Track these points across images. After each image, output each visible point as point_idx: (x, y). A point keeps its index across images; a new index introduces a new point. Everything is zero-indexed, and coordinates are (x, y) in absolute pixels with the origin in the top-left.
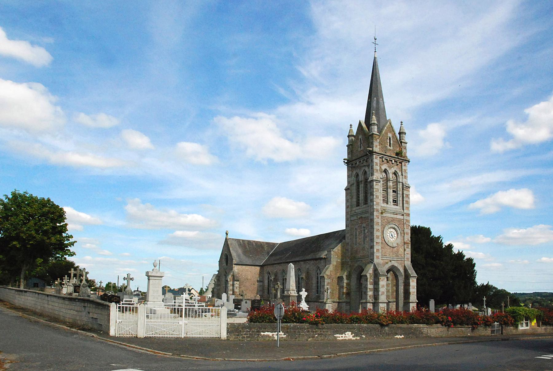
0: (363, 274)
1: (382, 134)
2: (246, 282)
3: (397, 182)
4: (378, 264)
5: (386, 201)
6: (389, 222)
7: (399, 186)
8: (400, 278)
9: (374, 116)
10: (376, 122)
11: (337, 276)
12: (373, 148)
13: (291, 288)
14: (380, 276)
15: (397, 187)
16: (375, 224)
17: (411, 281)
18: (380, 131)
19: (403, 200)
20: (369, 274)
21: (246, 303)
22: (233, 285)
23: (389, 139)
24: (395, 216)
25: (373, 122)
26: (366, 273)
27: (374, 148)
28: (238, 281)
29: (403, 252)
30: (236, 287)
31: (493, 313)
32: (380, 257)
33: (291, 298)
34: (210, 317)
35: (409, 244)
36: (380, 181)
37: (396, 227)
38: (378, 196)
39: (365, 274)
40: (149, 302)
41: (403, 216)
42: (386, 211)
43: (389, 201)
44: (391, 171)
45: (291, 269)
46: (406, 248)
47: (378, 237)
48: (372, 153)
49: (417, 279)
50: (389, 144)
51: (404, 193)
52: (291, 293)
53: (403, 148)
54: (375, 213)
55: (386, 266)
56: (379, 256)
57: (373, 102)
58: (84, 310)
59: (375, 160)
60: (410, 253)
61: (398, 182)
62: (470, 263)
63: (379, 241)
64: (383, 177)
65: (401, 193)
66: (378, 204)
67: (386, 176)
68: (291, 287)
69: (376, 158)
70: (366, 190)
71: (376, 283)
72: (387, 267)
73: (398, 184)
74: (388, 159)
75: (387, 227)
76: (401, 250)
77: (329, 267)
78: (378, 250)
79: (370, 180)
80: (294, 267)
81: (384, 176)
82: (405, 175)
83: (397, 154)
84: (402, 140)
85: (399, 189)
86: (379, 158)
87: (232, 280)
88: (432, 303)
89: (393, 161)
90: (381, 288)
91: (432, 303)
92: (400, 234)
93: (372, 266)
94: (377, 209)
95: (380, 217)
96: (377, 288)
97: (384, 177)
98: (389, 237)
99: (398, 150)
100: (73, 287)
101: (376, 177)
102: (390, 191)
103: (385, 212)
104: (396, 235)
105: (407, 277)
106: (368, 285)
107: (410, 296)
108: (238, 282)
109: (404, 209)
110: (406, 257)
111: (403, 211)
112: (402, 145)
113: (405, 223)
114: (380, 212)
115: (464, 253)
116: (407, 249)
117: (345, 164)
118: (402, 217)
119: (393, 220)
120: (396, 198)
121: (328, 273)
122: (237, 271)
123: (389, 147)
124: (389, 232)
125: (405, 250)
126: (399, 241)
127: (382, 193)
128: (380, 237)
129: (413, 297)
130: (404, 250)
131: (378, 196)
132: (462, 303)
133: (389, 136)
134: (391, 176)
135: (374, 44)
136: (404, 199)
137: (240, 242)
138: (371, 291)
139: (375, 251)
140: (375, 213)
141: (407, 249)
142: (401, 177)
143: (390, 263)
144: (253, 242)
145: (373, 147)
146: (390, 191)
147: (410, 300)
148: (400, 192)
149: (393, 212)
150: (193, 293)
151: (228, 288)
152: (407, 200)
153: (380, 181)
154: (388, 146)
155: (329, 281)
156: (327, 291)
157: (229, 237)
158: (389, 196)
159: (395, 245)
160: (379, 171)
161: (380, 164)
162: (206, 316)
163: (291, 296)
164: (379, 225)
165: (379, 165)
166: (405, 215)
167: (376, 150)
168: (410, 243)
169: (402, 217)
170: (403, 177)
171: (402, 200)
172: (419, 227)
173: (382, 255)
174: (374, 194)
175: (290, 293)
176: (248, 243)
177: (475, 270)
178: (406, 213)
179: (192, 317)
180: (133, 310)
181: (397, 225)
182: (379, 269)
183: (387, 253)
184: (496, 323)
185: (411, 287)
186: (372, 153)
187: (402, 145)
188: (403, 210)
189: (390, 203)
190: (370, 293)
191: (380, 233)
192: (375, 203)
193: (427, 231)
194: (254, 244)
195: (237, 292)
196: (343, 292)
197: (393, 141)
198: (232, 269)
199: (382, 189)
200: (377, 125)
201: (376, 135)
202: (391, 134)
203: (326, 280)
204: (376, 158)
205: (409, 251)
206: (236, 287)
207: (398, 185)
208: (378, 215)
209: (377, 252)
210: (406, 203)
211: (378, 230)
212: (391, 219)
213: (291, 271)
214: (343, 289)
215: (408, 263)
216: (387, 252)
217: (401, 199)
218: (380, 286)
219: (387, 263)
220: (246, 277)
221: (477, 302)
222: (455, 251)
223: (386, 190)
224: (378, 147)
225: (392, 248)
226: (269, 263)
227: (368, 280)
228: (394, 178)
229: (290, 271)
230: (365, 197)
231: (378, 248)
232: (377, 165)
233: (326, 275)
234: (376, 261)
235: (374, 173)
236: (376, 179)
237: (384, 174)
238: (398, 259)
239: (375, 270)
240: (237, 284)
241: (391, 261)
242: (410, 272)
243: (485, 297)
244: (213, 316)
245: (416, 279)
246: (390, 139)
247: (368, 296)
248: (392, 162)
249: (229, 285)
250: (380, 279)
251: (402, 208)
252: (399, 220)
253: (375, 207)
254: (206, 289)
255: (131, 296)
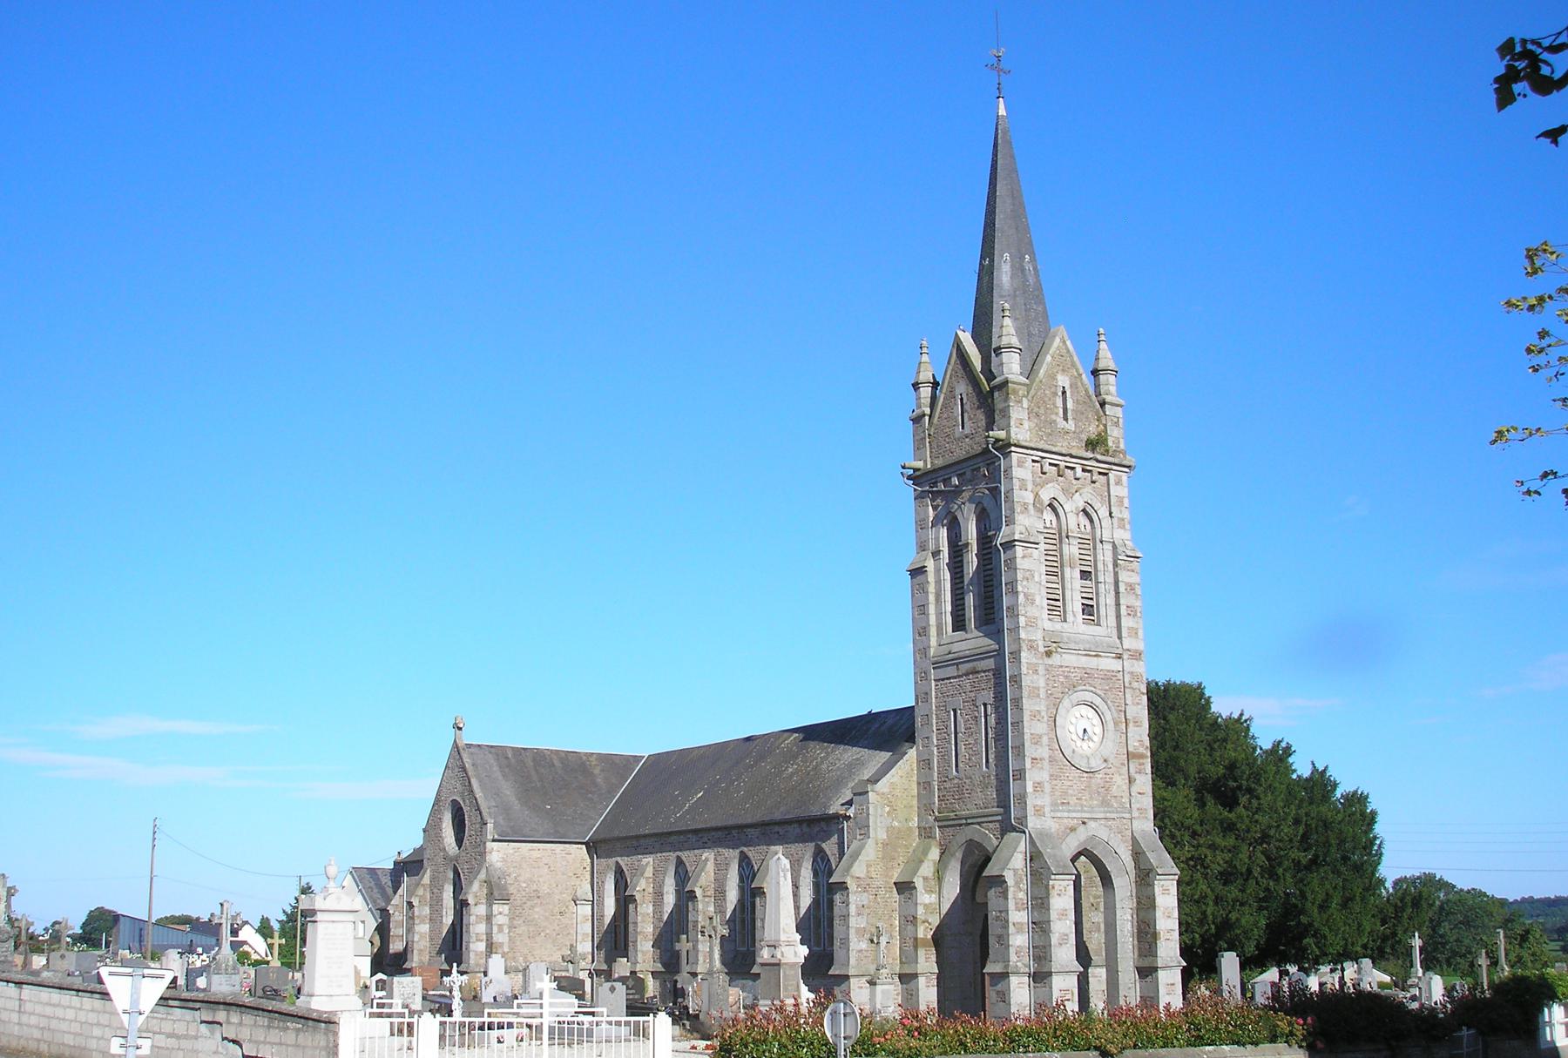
0: (991, 870)
1: (1037, 380)
2: (533, 907)
3: (1091, 543)
4: (1045, 835)
5: (1057, 606)
6: (1072, 684)
7: (1100, 557)
8: (1117, 882)
9: (1007, 321)
10: (1015, 341)
11: (893, 881)
12: (1007, 428)
13: (783, 937)
14: (1053, 877)
15: (1095, 561)
16: (1025, 693)
17: (1157, 890)
18: (1030, 372)
19: (1118, 605)
20: (1011, 872)
21: (612, 992)
22: (489, 918)
23: (1060, 394)
24: (1093, 663)
25: (1005, 341)
26: (1003, 869)
27: (1013, 430)
28: (506, 899)
29: (1125, 787)
30: (500, 927)
31: (1449, 991)
32: (1047, 810)
33: (784, 973)
34: (515, 1044)
35: (1147, 757)
36: (1037, 544)
37: (1098, 701)
38: (1033, 595)
39: (997, 874)
40: (314, 998)
41: (1121, 661)
42: (1061, 645)
43: (1069, 608)
44: (1071, 506)
45: (782, 874)
46: (1136, 773)
47: (1037, 740)
48: (1004, 447)
49: (1179, 883)
50: (1061, 411)
51: (1120, 579)
52: (783, 956)
53: (1109, 424)
54: (1025, 656)
55: (1068, 840)
56: (1043, 807)
57: (1000, 268)
58: (208, 1034)
59: (1017, 472)
60: (1148, 789)
61: (1098, 541)
62: (1358, 812)
63: (1043, 752)
64: (1045, 528)
65: (1110, 579)
66: (1032, 623)
67: (1054, 522)
68: (781, 933)
69: (1021, 464)
70: (987, 578)
71: (1040, 903)
72: (1071, 846)
73: (1099, 545)
74: (1062, 464)
75: (1066, 702)
76: (1120, 781)
77: (862, 847)
78: (1038, 786)
79: (1003, 541)
80: (788, 867)
81: (1048, 525)
82: (1120, 516)
83: (1092, 444)
84: (1104, 396)
85: (1100, 566)
86: (1029, 463)
87: (484, 901)
88: (1229, 963)
89: (1079, 469)
90: (1058, 921)
91: (1229, 963)
92: (1111, 725)
93: (1023, 843)
94: (1030, 641)
95: (1041, 670)
96: (1044, 922)
97: (1049, 528)
98: (1074, 737)
99: (1092, 430)
100: (295, 974)
101: (1024, 531)
102: (1072, 576)
103: (1059, 650)
104: (1098, 730)
105: (1145, 876)
106: (1010, 912)
107: (1159, 945)
108: (506, 907)
109: (1123, 635)
110: (1138, 806)
111: (1118, 641)
112: (1104, 412)
113: (1127, 685)
114: (1042, 649)
115: (1334, 773)
116: (1137, 776)
117: (907, 481)
118: (1115, 665)
119: (1088, 675)
120: (1092, 599)
121: (859, 869)
122: (499, 865)
123: (1061, 423)
124: (1074, 720)
125: (1131, 781)
126: (1112, 748)
127: (1044, 583)
128: (1045, 740)
129: (1169, 948)
130: (1127, 781)
131: (1033, 595)
132: (1339, 959)
133: (1060, 383)
134: (1074, 522)
135: (995, 73)
136: (1122, 602)
137: (507, 758)
138: (1019, 931)
139: (1030, 789)
140: (1023, 654)
141: (1137, 776)
142: (1106, 522)
143: (1082, 828)
144: (553, 756)
145: (1009, 426)
146: (1072, 576)
147: (1159, 959)
148: (1106, 577)
149: (1087, 647)
150: (249, 942)
151: (468, 932)
152: (1129, 604)
153: (1037, 544)
154: (1058, 420)
155: (865, 898)
156: (878, 938)
157: (467, 738)
158: (1068, 594)
159: (1096, 764)
160: (1031, 507)
161: (1035, 484)
162: (502, 1040)
163: (785, 964)
164: (1038, 696)
165: (1030, 487)
166: (1125, 657)
167: (1019, 436)
168: (1149, 754)
169: (1115, 665)
170: (1115, 525)
171: (1114, 603)
172: (1441, 879)
173: (1054, 804)
174: (1020, 589)
175: (779, 956)
176: (534, 760)
177: (1375, 838)
178: (1128, 650)
179: (462, 1045)
180: (400, 1032)
181: (1099, 692)
182: (1047, 852)
183: (1072, 795)
184: (1465, 1032)
185: (1159, 914)
186: (1004, 447)
187: (1107, 413)
188: (1120, 638)
189: (1075, 616)
190: (1019, 940)
191: (1045, 725)
192: (1022, 620)
193: (1371, 819)
194: (557, 763)
195: (501, 945)
196: (916, 939)
197: (1077, 402)
198: (483, 854)
199: (1043, 569)
200: (1020, 350)
201: (1020, 384)
202: (1067, 378)
203: (852, 898)
204: (1021, 464)
205: (1145, 782)
206: (500, 927)
207: (1099, 551)
208: (1034, 661)
209: (1037, 794)
210: (1129, 615)
211: (1035, 715)
212: (1079, 674)
213: (782, 879)
214: (915, 925)
215: (1146, 825)
216: (1070, 792)
217: (1111, 600)
218: (1053, 915)
219: (1073, 829)
220: (535, 887)
221: (1385, 950)
222: (1301, 767)
223: (1055, 571)
224: (1026, 424)
225: (1085, 775)
226: (616, 833)
227: (1010, 896)
228: (1083, 528)
229: (778, 883)
230: (986, 598)
231: (1038, 780)
232: (1023, 487)
233: (852, 877)
234: (1033, 823)
235: (1016, 514)
236: (1022, 537)
237: (1049, 516)
238: (1108, 815)
239: (1035, 856)
240: (500, 913)
241: (1084, 823)
242: (1152, 858)
243: (1417, 934)
244: (522, 1040)
245: (1175, 882)
246: (1064, 393)
247: (1012, 950)
248: (1075, 474)
249: (473, 919)
250: (1053, 888)
251: (1115, 632)
252: (1109, 676)
253: (1023, 635)
254: (279, 922)
255: (233, 976)
